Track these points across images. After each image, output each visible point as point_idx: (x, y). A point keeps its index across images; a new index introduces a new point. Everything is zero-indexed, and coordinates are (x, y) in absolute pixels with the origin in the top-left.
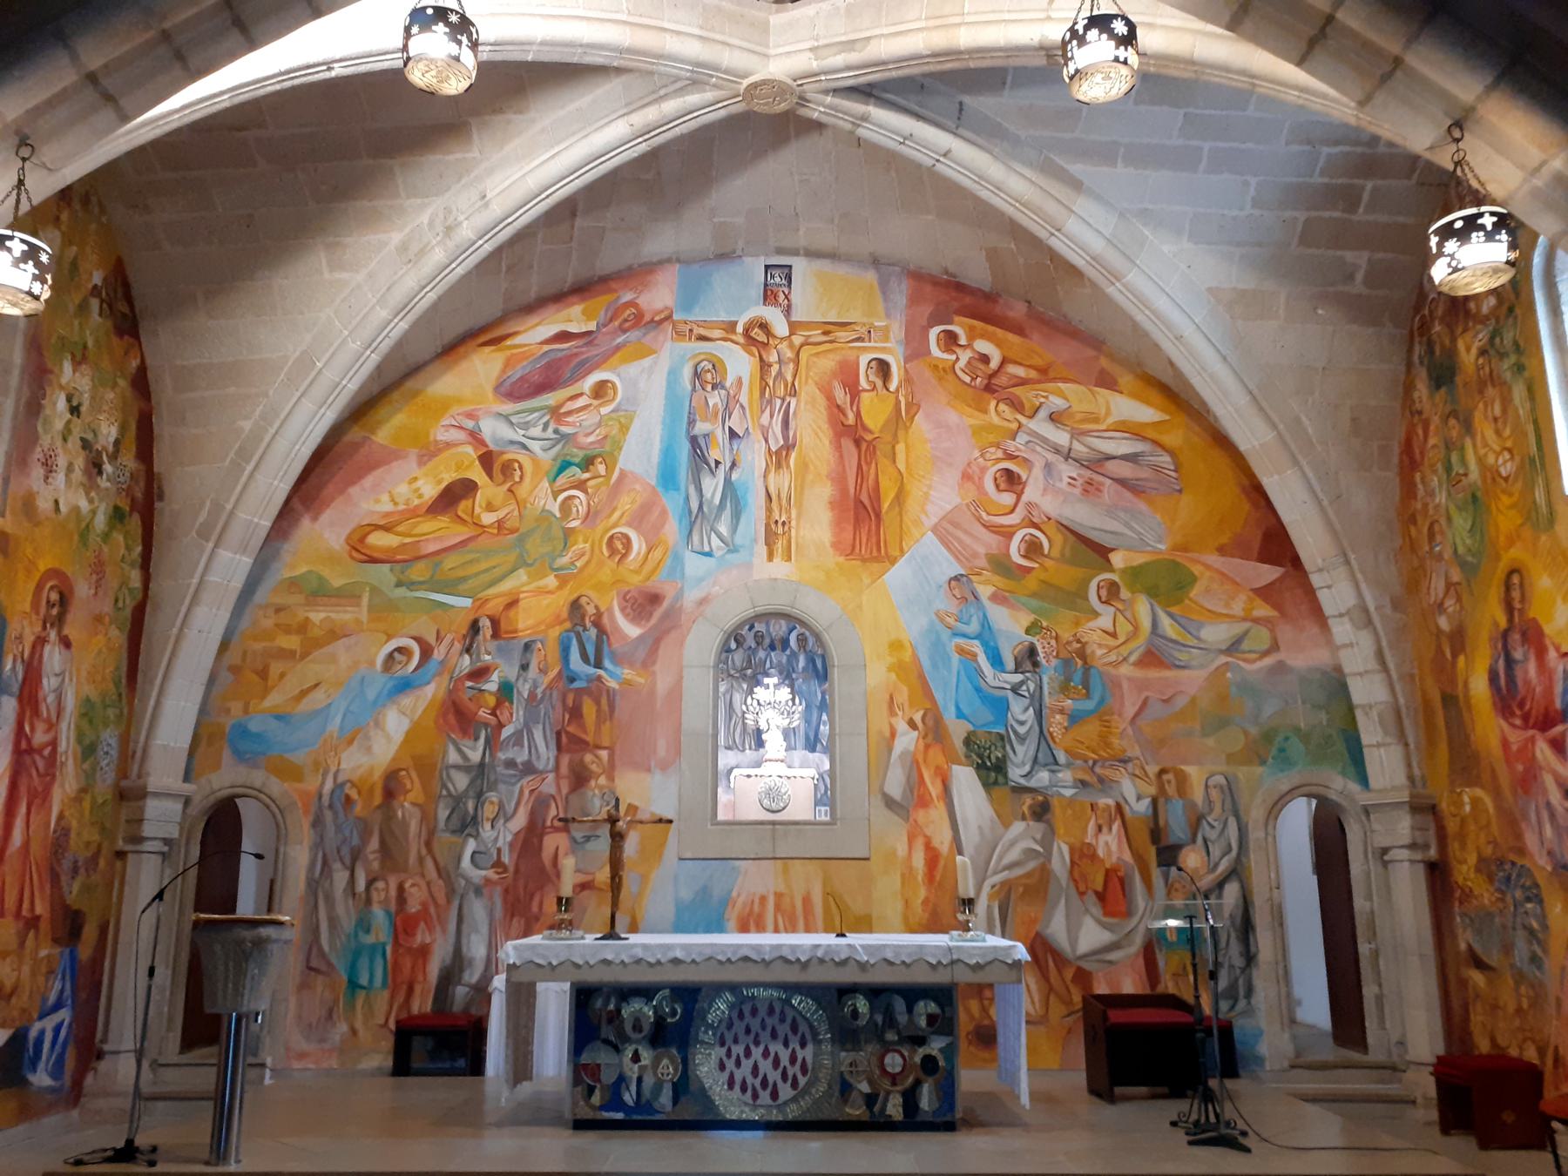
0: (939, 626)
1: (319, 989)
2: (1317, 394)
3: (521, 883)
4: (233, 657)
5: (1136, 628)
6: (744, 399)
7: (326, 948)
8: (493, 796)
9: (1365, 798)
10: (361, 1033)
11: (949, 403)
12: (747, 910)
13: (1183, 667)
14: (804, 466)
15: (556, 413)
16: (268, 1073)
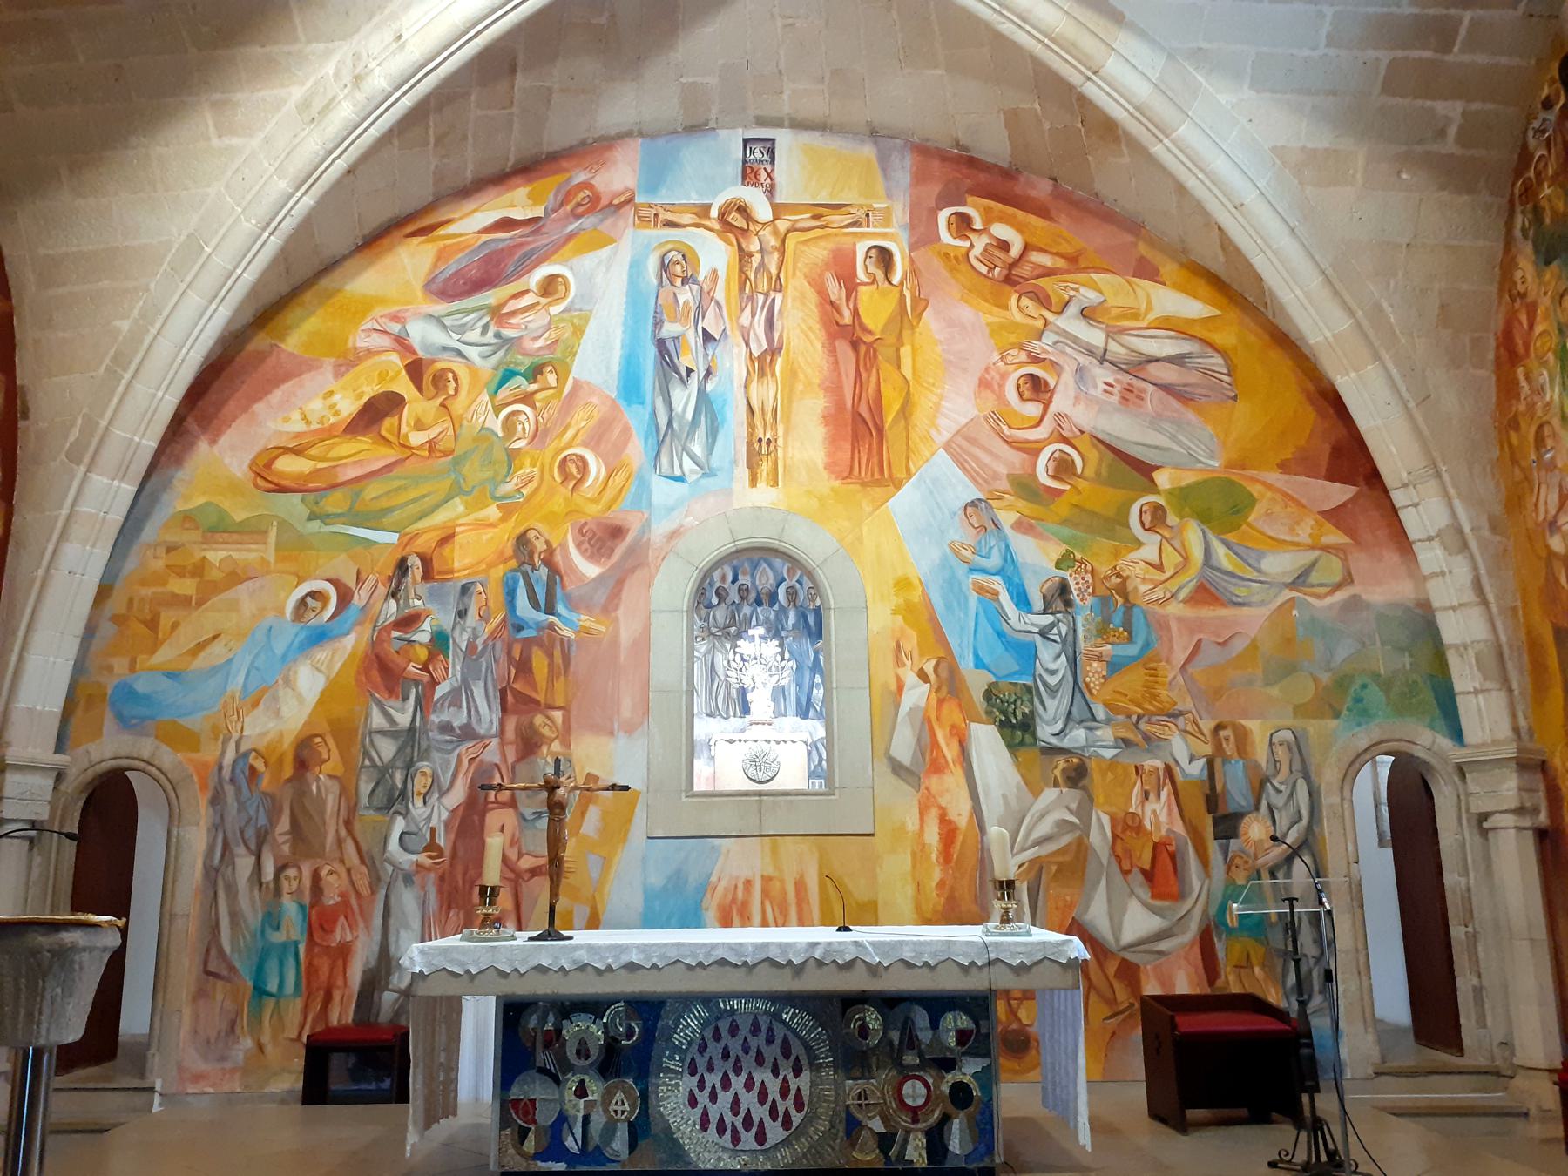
0: (954, 561)
1: (219, 996)
2: (1400, 274)
3: (459, 869)
4: (116, 604)
5: (1186, 559)
6: (720, 295)
7: (227, 948)
8: (425, 766)
9: (1456, 754)
10: (269, 1049)
11: (962, 298)
12: (730, 897)
13: (1240, 604)
14: (792, 373)
15: (497, 314)
16: (157, 1099)
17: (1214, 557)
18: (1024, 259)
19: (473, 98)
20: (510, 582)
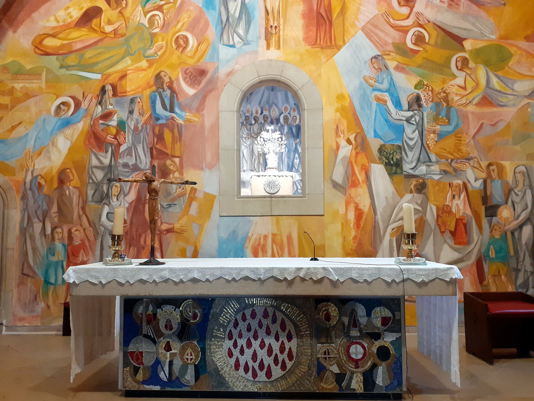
0: (365, 85)
1: (29, 285)
3: (134, 229)
5: (478, 84)
7: (32, 263)
10: (52, 307)
12: (257, 243)
17: (491, 84)
20: (153, 97)
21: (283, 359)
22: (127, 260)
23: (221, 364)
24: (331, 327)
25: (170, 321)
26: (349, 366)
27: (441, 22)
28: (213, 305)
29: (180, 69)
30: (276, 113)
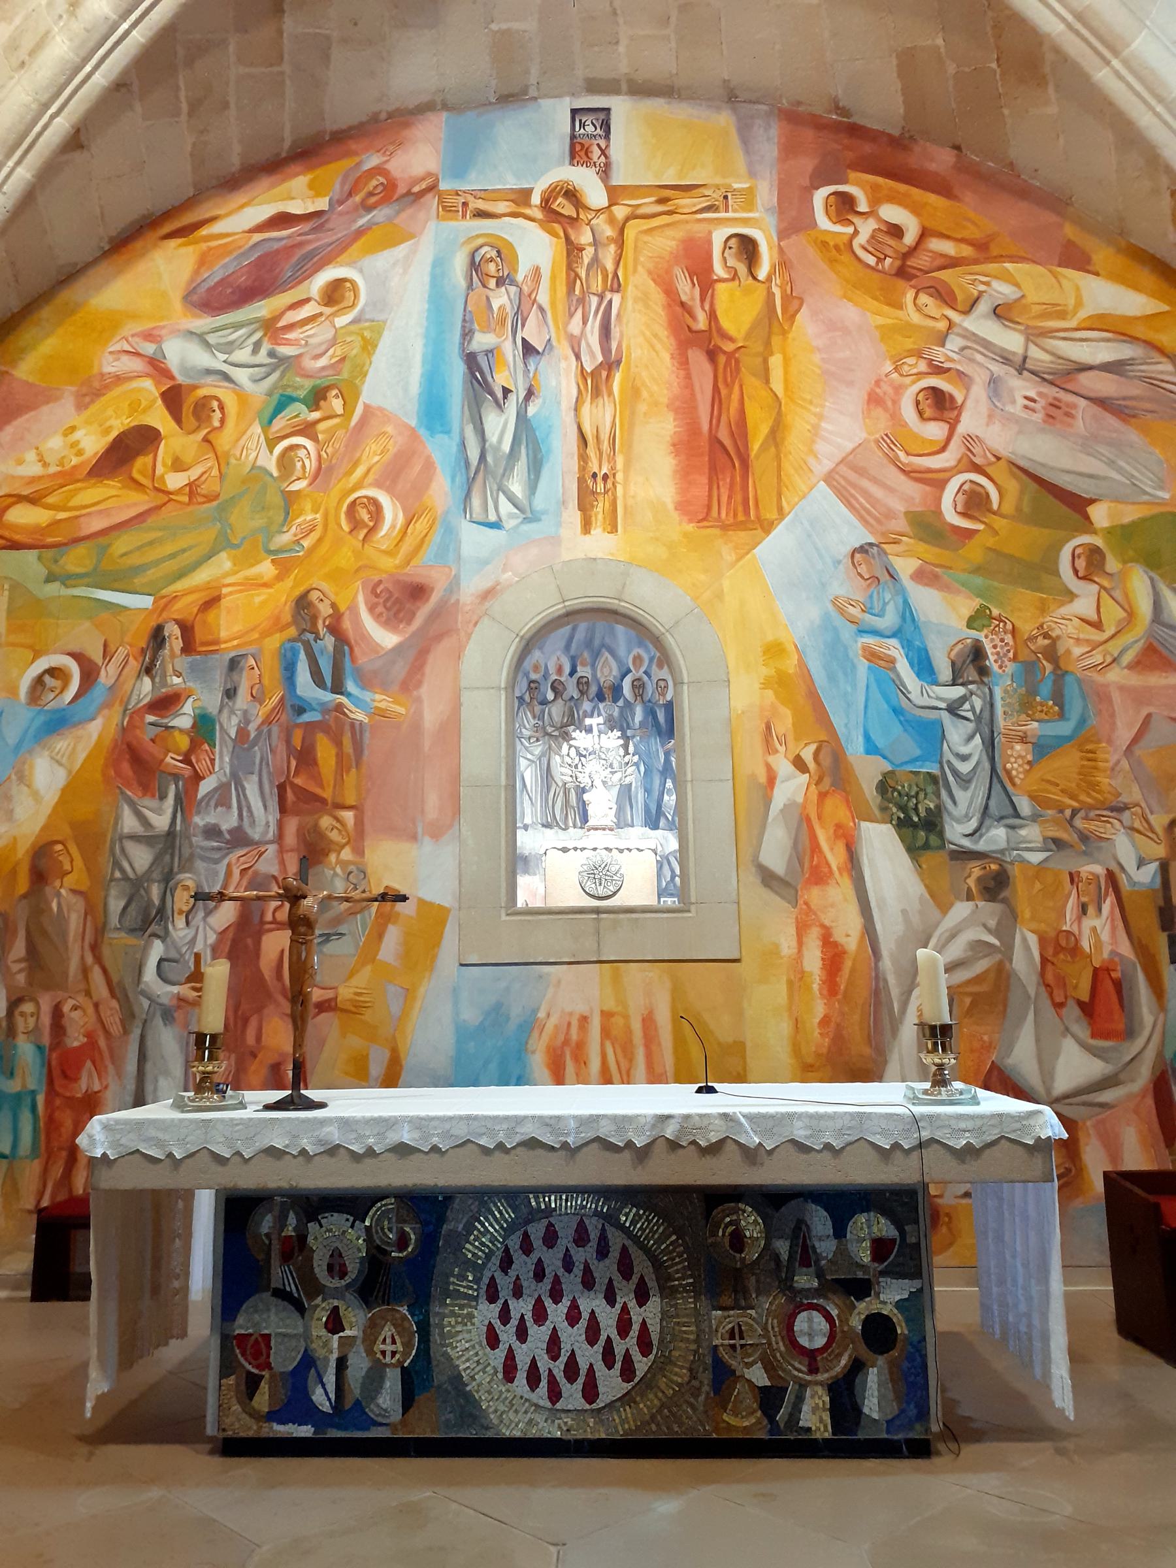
0: (839, 621)
5: (1131, 614)
6: (543, 298)
12: (561, 1037)
14: (633, 392)
15: (271, 328)
18: (923, 246)
19: (231, 48)
20: (289, 655)
21: (627, 1350)
22: (231, 1097)
23: (468, 1364)
24: (747, 1266)
25: (340, 1255)
26: (793, 1366)
27: (1031, 460)
28: (449, 1213)
29: (359, 583)
30: (611, 670)
